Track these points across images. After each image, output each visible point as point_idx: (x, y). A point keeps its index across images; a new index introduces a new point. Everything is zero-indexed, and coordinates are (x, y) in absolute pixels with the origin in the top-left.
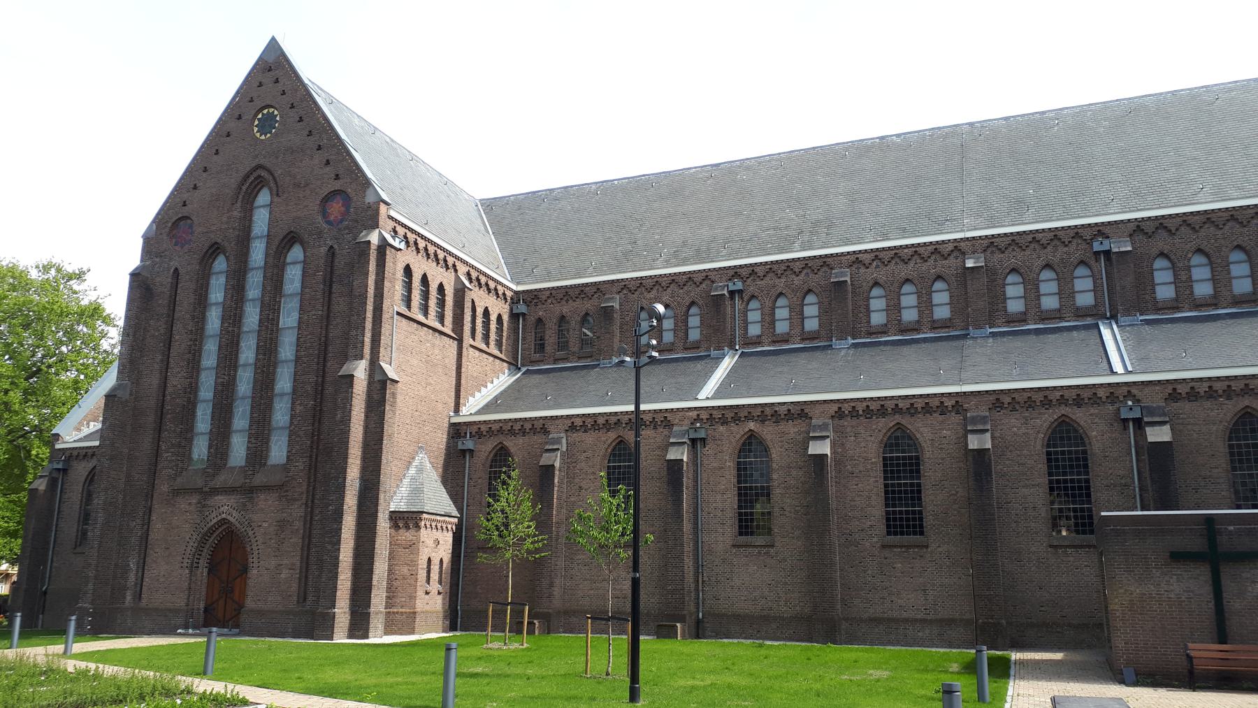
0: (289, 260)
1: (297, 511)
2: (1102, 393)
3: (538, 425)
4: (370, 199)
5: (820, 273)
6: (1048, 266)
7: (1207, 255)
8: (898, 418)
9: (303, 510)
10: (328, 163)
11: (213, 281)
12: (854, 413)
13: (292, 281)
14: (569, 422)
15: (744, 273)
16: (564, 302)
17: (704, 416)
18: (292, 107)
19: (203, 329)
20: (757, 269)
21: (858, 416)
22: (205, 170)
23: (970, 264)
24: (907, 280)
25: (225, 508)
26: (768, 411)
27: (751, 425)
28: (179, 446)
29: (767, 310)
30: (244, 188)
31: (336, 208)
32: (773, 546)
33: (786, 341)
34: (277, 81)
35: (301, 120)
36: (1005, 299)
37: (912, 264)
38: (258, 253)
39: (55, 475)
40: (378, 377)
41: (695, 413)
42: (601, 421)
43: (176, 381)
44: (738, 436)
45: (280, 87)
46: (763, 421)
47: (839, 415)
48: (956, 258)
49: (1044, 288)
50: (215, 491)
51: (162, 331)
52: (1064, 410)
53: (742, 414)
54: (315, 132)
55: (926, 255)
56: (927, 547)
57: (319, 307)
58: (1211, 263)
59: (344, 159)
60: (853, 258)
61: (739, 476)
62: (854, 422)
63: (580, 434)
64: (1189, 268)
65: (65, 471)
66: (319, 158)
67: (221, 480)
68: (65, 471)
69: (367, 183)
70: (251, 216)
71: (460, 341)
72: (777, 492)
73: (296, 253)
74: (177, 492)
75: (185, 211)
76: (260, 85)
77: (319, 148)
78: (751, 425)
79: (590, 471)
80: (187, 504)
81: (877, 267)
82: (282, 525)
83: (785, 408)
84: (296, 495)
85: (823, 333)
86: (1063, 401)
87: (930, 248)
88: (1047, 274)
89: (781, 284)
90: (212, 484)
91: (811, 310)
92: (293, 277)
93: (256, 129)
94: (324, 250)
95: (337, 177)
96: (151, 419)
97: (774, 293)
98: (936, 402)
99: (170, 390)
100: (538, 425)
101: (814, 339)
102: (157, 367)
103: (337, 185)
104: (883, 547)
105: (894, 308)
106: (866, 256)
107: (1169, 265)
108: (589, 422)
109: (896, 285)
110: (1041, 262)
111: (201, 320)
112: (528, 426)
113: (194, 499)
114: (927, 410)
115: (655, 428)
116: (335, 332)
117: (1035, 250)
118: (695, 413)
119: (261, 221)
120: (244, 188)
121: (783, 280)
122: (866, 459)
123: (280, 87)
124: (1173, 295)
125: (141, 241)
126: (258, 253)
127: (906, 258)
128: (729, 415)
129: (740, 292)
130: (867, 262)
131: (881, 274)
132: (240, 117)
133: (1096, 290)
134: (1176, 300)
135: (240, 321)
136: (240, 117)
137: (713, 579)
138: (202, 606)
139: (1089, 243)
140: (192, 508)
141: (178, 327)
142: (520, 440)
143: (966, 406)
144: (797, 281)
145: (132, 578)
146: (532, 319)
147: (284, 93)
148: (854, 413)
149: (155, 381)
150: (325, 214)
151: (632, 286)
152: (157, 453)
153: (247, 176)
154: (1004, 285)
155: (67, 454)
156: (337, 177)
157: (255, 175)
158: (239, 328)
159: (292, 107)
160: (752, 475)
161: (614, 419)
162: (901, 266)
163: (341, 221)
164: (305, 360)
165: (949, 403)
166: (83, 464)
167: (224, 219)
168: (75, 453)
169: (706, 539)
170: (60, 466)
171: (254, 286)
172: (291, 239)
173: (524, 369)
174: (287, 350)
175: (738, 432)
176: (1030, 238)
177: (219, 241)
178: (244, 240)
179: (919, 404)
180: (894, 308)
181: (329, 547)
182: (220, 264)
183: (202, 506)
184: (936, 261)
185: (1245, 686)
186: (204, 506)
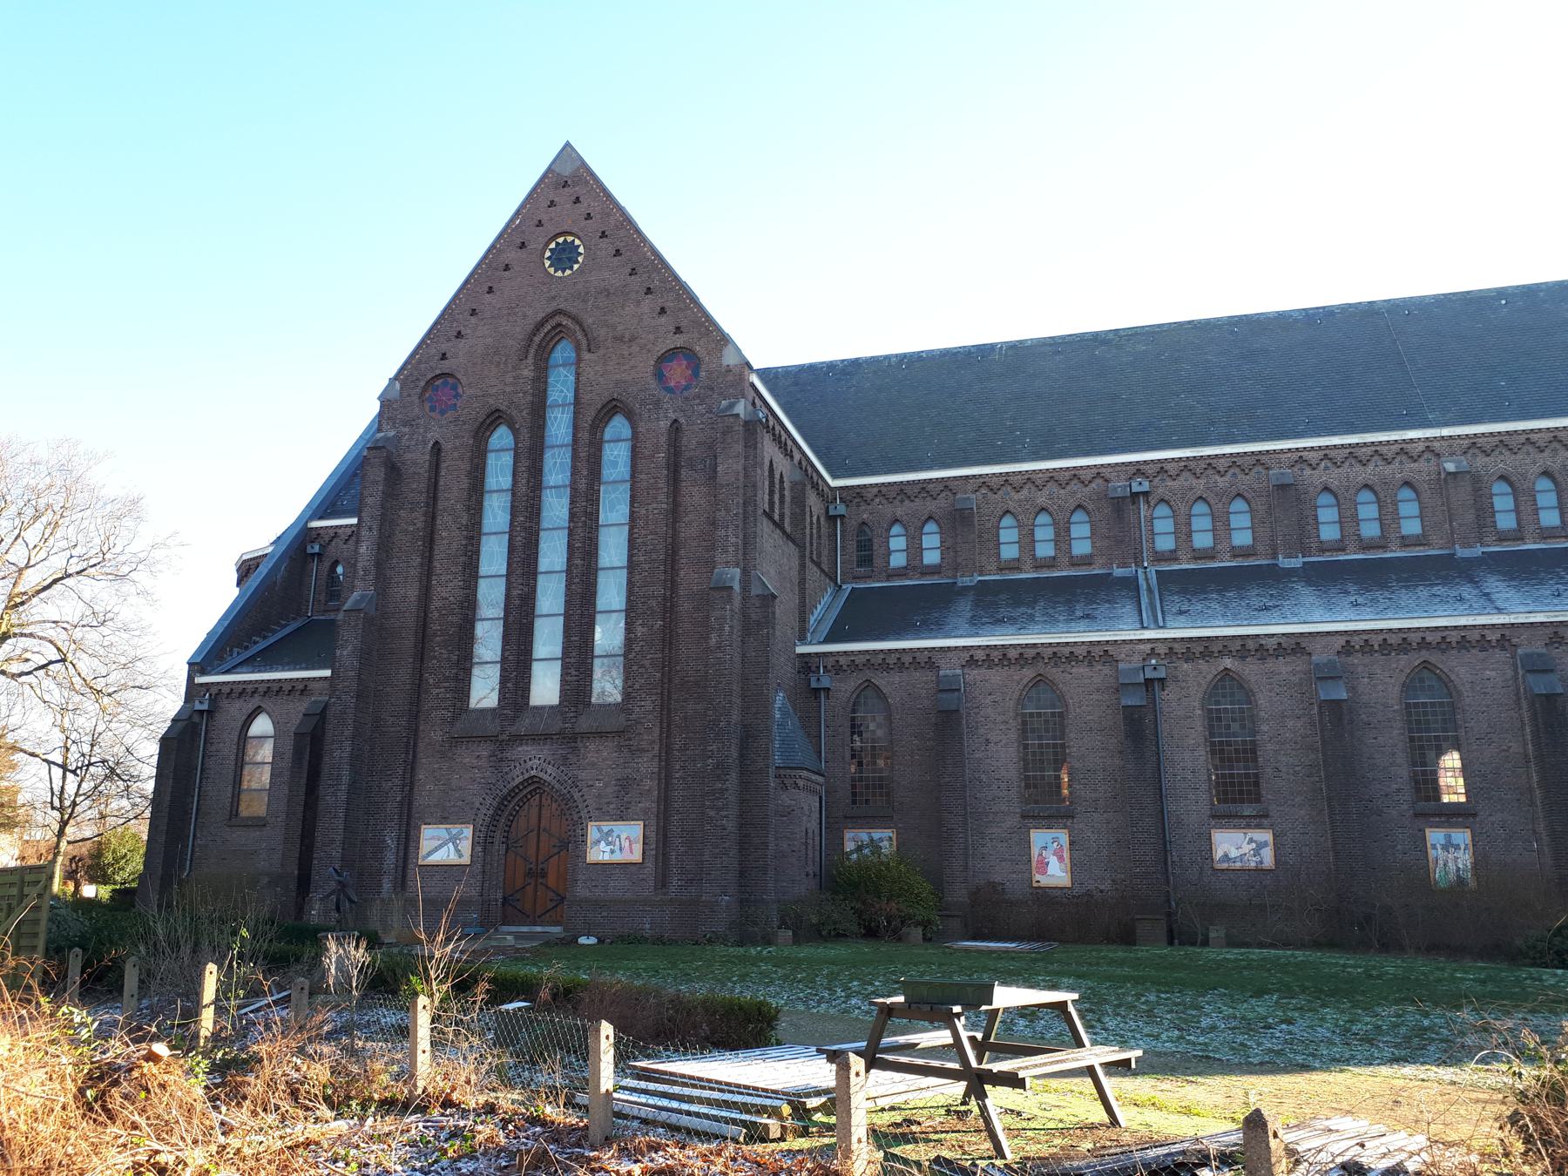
0: (607, 436)
1: (647, 765)
3: (922, 658)
4: (729, 359)
5: (1252, 473)
7: (1511, 484)
8: (1424, 655)
9: (655, 764)
10: (663, 311)
11: (491, 459)
12: (1367, 648)
13: (615, 464)
14: (966, 656)
15: (1150, 470)
16: (897, 502)
17: (1162, 649)
18: (603, 235)
19: (480, 523)
20: (1168, 467)
21: (1372, 651)
22: (473, 312)
23: (1450, 467)
24: (1366, 486)
25: (534, 760)
26: (1251, 645)
27: (1228, 662)
28: (456, 678)
29: (1182, 519)
30: (537, 339)
31: (677, 372)
32: (1267, 816)
33: (1213, 558)
34: (577, 201)
35: (618, 253)
36: (1493, 513)
37: (1371, 467)
38: (559, 426)
39: (196, 719)
40: (756, 590)
41: (1149, 646)
42: (1013, 654)
43: (446, 590)
44: (1210, 677)
45: (582, 208)
46: (1243, 658)
47: (1347, 649)
48: (1428, 460)
49: (1040, 534)
50: (518, 739)
51: (419, 525)
53: (1215, 648)
54: (640, 270)
55: (1390, 456)
56: (1475, 815)
57: (662, 497)
58: (1379, 501)
59: (688, 307)
60: (1295, 456)
61: (1211, 727)
62: (1367, 659)
63: (983, 671)
64: (1395, 503)
65: (210, 712)
66: (648, 305)
67: (524, 725)
69: (723, 340)
70: (546, 377)
72: (1267, 750)
73: (618, 426)
74: (456, 741)
75: (446, 366)
76: (552, 204)
77: (649, 291)
78: (1228, 662)
79: (999, 719)
80: (473, 758)
81: (1326, 468)
82: (625, 785)
83: (1274, 641)
84: (644, 744)
85: (1260, 548)
87: (1396, 448)
89: (1200, 485)
90: (513, 730)
91: (1081, 530)
92: (616, 457)
93: (547, 263)
94: (664, 424)
95: (678, 330)
96: (408, 643)
97: (1191, 496)
98: (1476, 635)
99: (436, 603)
100: (922, 658)
101: (1249, 555)
102: (413, 572)
103: (680, 341)
104: (1416, 815)
106: (1312, 454)
107: (1509, 490)
108: (996, 655)
109: (1352, 491)
110: (1536, 469)
112: (907, 659)
113: (484, 750)
115: (1090, 665)
116: (690, 529)
117: (1528, 454)
118: (1149, 646)
119: (561, 386)
120: (537, 339)
121: (1202, 481)
122: (1386, 706)
123: (582, 208)
124: (1338, 536)
125: (375, 408)
126: (559, 426)
127: (1364, 458)
128: (1198, 649)
129: (1146, 494)
130: (1314, 462)
131: (1334, 477)
132: (523, 246)
134: (1383, 536)
135: (539, 514)
136: (523, 246)
137: (1186, 859)
138: (500, 895)
140: (483, 763)
141: (443, 520)
142: (896, 678)
143: (1514, 641)
144: (1222, 482)
145: (390, 859)
146: (853, 524)
147: (589, 217)
148: (1367, 648)
149: (413, 592)
150: (659, 376)
151: (994, 483)
152: (419, 687)
153: (541, 324)
154: (1491, 496)
155: (214, 691)
156: (678, 330)
157: (553, 322)
158: (538, 523)
159: (603, 235)
160: (1228, 727)
161: (1032, 652)
162: (1358, 468)
163: (687, 388)
164: (646, 567)
165: (1493, 637)
166: (238, 704)
167: (509, 379)
168: (226, 690)
169: (1172, 807)
170: (205, 707)
172: (611, 408)
173: (848, 587)
175: (1208, 670)
176: (1522, 438)
177: (503, 408)
181: (712, 813)
182: (502, 437)
183: (498, 761)
184: (1401, 463)
186: (501, 760)
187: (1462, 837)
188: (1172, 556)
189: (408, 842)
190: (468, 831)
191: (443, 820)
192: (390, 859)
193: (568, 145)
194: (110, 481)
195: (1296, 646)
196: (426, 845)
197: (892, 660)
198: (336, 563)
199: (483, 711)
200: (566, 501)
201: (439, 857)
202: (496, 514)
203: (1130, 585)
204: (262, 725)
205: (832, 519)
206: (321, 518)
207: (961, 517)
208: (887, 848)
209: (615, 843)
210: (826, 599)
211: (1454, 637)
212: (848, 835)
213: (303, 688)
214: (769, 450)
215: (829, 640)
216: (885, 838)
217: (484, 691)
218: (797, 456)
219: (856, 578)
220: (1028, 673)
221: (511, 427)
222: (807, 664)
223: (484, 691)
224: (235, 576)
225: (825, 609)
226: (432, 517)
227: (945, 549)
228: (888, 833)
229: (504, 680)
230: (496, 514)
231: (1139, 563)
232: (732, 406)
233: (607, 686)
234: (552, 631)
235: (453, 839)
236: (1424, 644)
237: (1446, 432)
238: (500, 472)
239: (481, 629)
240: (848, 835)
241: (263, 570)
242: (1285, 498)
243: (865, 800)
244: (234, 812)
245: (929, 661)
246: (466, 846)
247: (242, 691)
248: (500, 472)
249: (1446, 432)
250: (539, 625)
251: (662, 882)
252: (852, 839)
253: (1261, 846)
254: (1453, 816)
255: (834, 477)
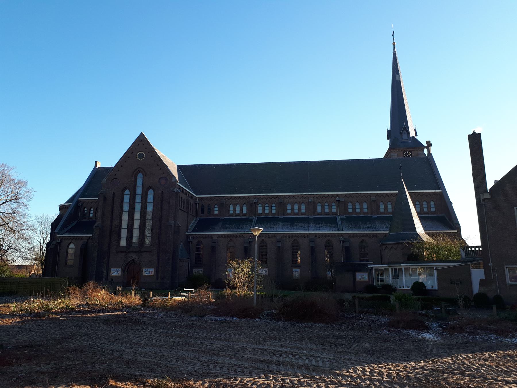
2: (336, 235)
6: (326, 202)
22: (122, 166)
23: (310, 200)
25: (133, 256)
27: (263, 238)
31: (163, 181)
36: (127, 237)
38: (139, 191)
52: (329, 238)
65: (60, 243)
68: (60, 243)
71: (188, 213)
86: (329, 236)
88: (326, 204)
92: (150, 198)
94: (160, 192)
103: (163, 175)
105: (293, 209)
111: (122, 207)
114: (301, 236)
119: (140, 182)
126: (139, 191)
133: (336, 209)
139: (336, 198)
145: (104, 275)
171: (138, 199)
173: (198, 218)
174: (149, 216)
178: (135, 187)
179: (300, 235)
180: (293, 209)
182: (127, 192)
185: (82, 382)
187: (298, 270)
188: (261, 214)
189: (108, 271)
190: (120, 269)
191: (115, 267)
192: (104, 275)
193: (142, 134)
194: (16, 175)
195: (274, 235)
196: (112, 272)
197: (288, 235)
198: (85, 208)
199: (123, 247)
200: (140, 206)
201: (114, 274)
202: (126, 207)
203: (252, 220)
204: (72, 246)
205: (196, 204)
206: (81, 197)
207: (223, 205)
208: (201, 272)
209: (148, 272)
210: (194, 221)
211: (294, 235)
212: (194, 270)
213: (82, 238)
214: (182, 195)
215: (193, 231)
216: (201, 270)
217: (123, 243)
218: (188, 194)
219: (201, 216)
220: (229, 239)
221: (129, 190)
222: (188, 237)
223: (123, 243)
224: (59, 208)
225: (193, 223)
226: (113, 208)
227: (218, 211)
228: (202, 269)
229: (127, 241)
230: (126, 207)
231: (254, 216)
232: (173, 189)
233: (147, 241)
234: (134, 223)
235: (117, 271)
236: (295, 236)
237: (310, 193)
238: (127, 199)
239: (123, 230)
240: (194, 270)
241: (69, 210)
242: (281, 204)
243: (198, 263)
244: (66, 264)
245: (211, 236)
246: (120, 272)
247: (68, 238)
248: (127, 199)
249: (310, 193)
250: (134, 230)
251: (157, 279)
252: (195, 270)
253: (266, 271)
254: (298, 266)
255: (197, 195)
